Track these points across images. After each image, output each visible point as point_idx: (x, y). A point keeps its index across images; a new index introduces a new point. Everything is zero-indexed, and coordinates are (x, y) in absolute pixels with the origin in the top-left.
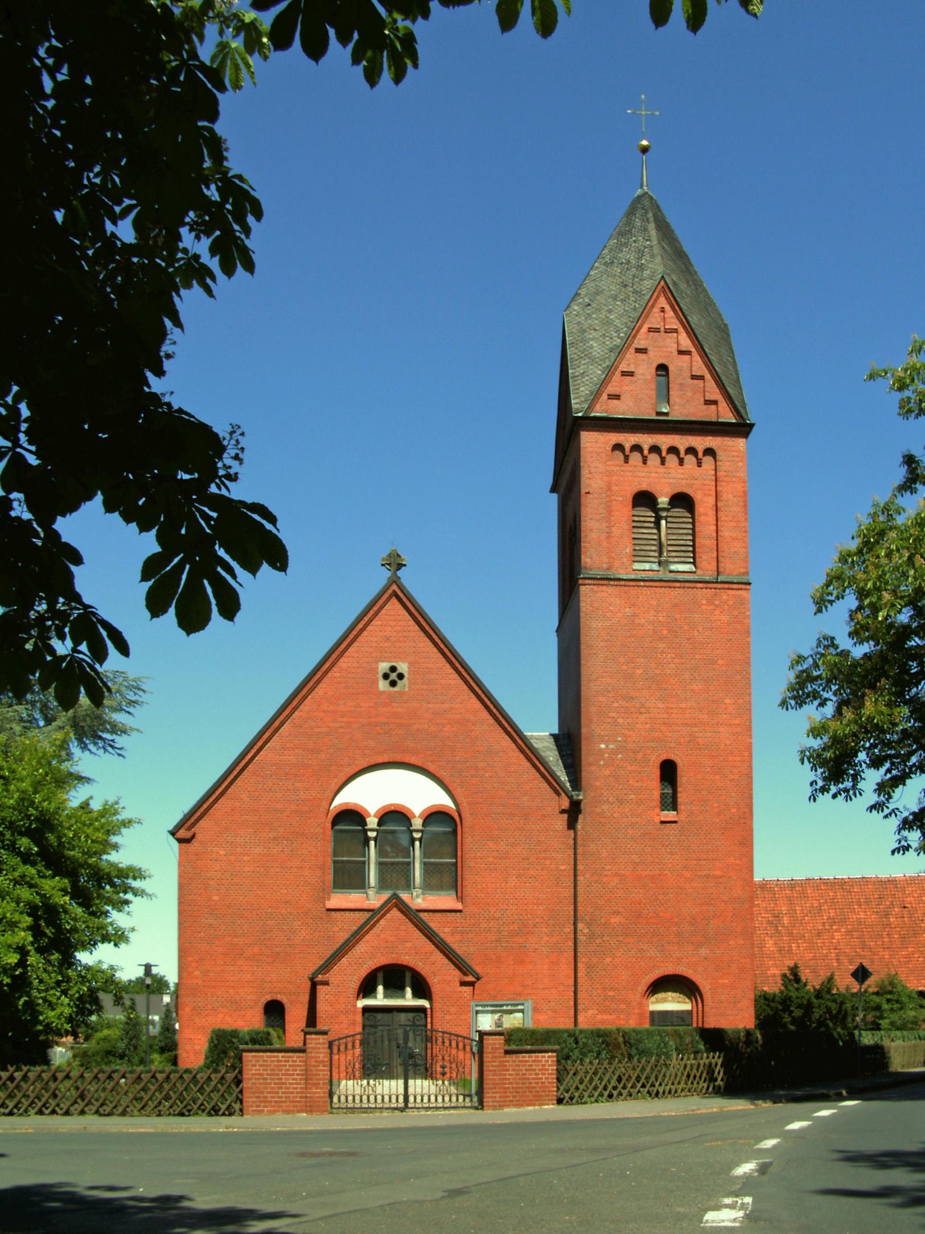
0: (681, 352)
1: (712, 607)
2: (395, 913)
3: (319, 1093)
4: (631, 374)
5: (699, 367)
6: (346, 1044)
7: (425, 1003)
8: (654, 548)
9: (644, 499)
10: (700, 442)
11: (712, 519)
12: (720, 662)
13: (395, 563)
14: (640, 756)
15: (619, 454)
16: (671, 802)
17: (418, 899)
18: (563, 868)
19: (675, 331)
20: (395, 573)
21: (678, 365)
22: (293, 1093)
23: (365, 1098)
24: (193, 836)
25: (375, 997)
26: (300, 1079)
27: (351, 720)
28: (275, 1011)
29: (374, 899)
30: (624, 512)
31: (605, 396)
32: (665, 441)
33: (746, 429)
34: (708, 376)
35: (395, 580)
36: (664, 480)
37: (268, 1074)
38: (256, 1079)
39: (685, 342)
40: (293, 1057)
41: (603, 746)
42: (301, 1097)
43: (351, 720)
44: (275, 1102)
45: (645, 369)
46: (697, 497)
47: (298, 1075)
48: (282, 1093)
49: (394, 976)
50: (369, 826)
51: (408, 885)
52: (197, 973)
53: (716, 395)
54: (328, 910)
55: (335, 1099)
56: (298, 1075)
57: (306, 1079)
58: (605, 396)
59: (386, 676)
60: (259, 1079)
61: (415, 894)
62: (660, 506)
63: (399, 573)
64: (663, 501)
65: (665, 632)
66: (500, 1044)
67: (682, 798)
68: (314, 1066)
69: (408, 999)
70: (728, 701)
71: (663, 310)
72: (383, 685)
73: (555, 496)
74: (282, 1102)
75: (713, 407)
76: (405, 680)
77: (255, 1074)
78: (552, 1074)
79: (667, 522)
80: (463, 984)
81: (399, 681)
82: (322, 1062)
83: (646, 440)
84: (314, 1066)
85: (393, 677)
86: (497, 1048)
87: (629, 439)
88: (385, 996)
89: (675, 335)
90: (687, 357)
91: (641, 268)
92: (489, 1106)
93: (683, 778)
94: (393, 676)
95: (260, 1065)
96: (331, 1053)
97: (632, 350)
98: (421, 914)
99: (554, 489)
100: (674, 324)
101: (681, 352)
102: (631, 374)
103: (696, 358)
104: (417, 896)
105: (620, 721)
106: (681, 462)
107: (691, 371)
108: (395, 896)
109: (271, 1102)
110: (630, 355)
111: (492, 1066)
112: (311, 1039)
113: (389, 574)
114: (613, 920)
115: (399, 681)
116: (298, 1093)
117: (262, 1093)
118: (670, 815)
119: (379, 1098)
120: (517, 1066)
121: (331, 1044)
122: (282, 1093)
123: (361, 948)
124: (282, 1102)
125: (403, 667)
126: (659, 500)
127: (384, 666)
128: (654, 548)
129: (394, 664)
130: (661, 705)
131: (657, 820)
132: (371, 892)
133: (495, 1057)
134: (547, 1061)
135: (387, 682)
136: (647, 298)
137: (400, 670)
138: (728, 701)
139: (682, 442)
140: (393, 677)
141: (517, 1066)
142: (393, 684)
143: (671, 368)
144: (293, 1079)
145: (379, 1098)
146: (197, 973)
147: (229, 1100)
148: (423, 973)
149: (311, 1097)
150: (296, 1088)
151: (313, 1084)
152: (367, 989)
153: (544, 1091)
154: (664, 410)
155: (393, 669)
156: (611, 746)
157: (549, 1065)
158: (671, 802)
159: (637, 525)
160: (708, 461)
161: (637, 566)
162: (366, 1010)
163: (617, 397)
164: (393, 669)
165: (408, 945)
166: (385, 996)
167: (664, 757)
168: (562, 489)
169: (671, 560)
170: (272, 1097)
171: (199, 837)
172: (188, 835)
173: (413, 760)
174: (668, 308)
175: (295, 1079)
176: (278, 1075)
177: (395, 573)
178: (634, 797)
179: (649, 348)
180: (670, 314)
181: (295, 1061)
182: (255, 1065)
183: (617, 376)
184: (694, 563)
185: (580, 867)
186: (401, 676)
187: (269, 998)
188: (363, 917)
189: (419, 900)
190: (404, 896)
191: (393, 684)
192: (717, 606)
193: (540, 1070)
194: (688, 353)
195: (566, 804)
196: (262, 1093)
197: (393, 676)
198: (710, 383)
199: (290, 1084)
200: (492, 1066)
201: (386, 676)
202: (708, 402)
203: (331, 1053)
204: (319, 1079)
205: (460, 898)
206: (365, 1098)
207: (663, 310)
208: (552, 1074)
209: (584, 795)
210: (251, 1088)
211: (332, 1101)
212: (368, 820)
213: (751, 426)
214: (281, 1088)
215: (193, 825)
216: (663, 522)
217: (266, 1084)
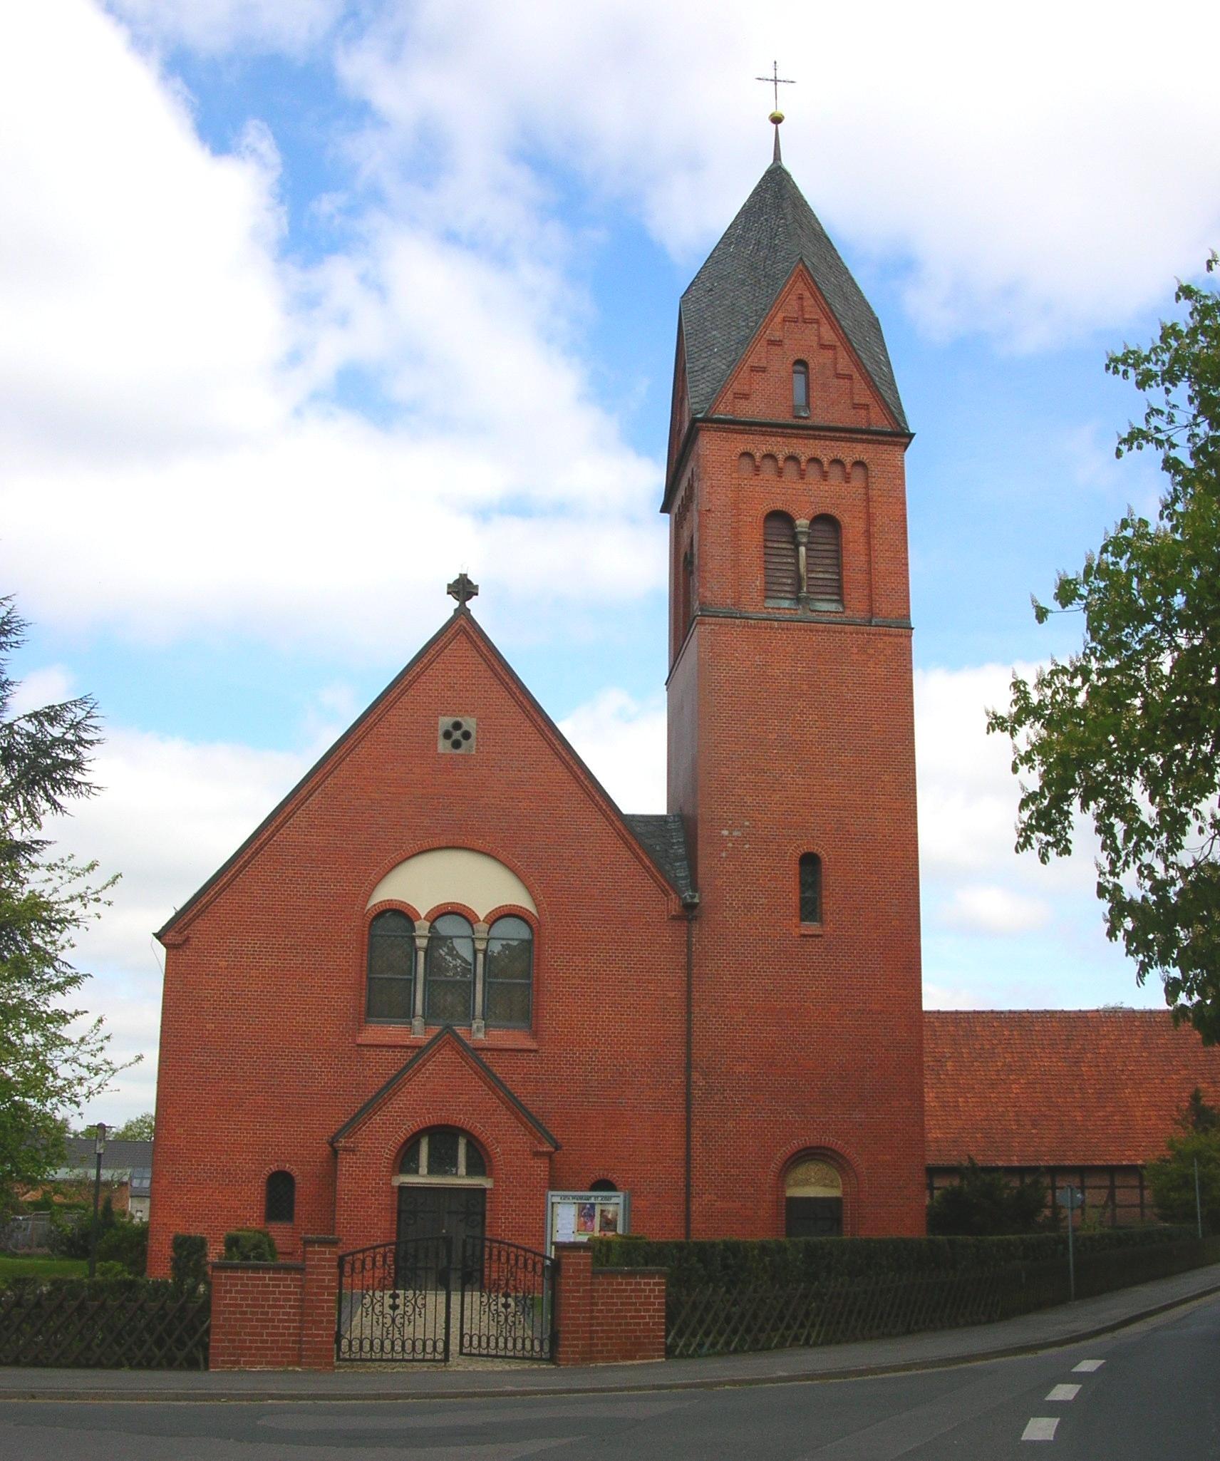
0: (823, 346)
1: (864, 657)
2: (447, 1054)
3: (321, 1336)
4: (763, 370)
5: (844, 364)
6: (363, 1262)
7: (486, 1183)
8: (789, 581)
9: (780, 518)
10: (850, 452)
11: (862, 548)
12: (876, 727)
13: (463, 589)
14: (773, 847)
15: (746, 461)
16: (810, 909)
17: (478, 1034)
18: (672, 995)
19: (817, 322)
20: (463, 604)
21: (817, 361)
22: (284, 1335)
23: (387, 1344)
24: (187, 939)
25: (416, 1172)
26: (295, 1314)
27: (401, 790)
28: (280, 1191)
29: (419, 1032)
30: (753, 537)
31: (730, 395)
32: (805, 449)
33: (906, 440)
34: (856, 375)
35: (462, 613)
36: (805, 498)
37: (248, 1306)
38: (230, 1312)
39: (828, 335)
40: (286, 1279)
41: (725, 833)
42: (294, 1342)
43: (401, 790)
44: (258, 1349)
45: (780, 364)
46: (845, 519)
47: (291, 1307)
48: (268, 1334)
49: (443, 1138)
50: (418, 933)
51: (468, 1015)
52: (179, 1130)
53: (863, 396)
54: (359, 1045)
55: (345, 1342)
56: (291, 1307)
57: (302, 1314)
58: (730, 395)
59: (447, 735)
60: (234, 1313)
61: (475, 1026)
62: (799, 529)
63: (468, 604)
64: (802, 523)
65: (805, 687)
66: (585, 1264)
67: (829, 905)
68: (316, 1294)
69: (460, 1178)
70: (886, 778)
71: (801, 298)
72: (443, 746)
73: (667, 516)
74: (267, 1348)
75: (863, 412)
76: (472, 740)
77: (231, 1305)
78: (659, 1310)
79: (807, 550)
80: (537, 1154)
81: (464, 742)
82: (327, 1288)
83: (781, 447)
84: (316, 1294)
85: (457, 735)
86: (581, 1271)
87: (760, 446)
88: (431, 1172)
89: (815, 326)
90: (830, 353)
91: (774, 249)
92: (568, 1360)
93: (832, 878)
94: (457, 735)
95: (237, 1292)
96: (341, 1274)
97: (763, 342)
98: (483, 1055)
99: (665, 509)
100: (812, 311)
101: (823, 346)
102: (763, 370)
103: (842, 353)
104: (478, 1029)
105: (748, 799)
106: (825, 476)
107: (836, 369)
108: (448, 1028)
109: (250, 1348)
110: (761, 348)
111: (574, 1298)
112: (314, 1253)
113: (456, 604)
114: (738, 1069)
115: (464, 742)
116: (290, 1335)
117: (238, 1334)
118: (812, 927)
119: (409, 1344)
120: (609, 1297)
121: (341, 1260)
122: (268, 1334)
123: (400, 1102)
124: (267, 1348)
125: (470, 723)
126: (798, 522)
127: (445, 722)
128: (789, 581)
129: (459, 719)
130: (800, 780)
131: (796, 932)
132: (418, 1023)
133: (578, 1284)
134: (651, 1290)
135: (448, 743)
136: (781, 283)
137: (465, 728)
138: (886, 778)
139: (825, 451)
140: (457, 735)
141: (609, 1297)
142: (457, 745)
143: (811, 365)
144: (284, 1314)
145: (409, 1344)
146: (179, 1130)
147: (190, 1344)
148: (483, 1138)
149: (308, 1342)
150: (288, 1328)
151: (314, 1322)
152: (405, 1159)
153: (648, 1337)
154: (803, 414)
155: (457, 726)
156: (735, 833)
157: (655, 1297)
158: (810, 909)
159: (768, 552)
160: (858, 474)
161: (770, 603)
162: (402, 1189)
163: (746, 396)
164: (457, 726)
165: (464, 1098)
166: (431, 1172)
167: (805, 849)
168: (675, 509)
169: (812, 596)
170: (251, 1341)
171: (194, 942)
172: (180, 939)
173: (479, 844)
174: (807, 294)
175: (288, 1314)
176: (263, 1306)
177: (463, 604)
178: (763, 901)
179: (786, 341)
180: (809, 302)
181: (289, 1286)
182: (230, 1292)
183: (745, 373)
184: (840, 601)
185: (696, 995)
186: (467, 735)
187: (274, 1168)
188: (403, 1057)
189: (481, 1036)
190: (460, 1030)
191: (457, 745)
192: (871, 656)
193: (641, 1304)
194: (833, 348)
195: (675, 907)
196: (238, 1334)
197: (457, 735)
198: (860, 385)
199: (280, 1321)
200: (574, 1298)
201: (447, 735)
202: (856, 406)
203: (341, 1274)
204: (322, 1315)
205: (535, 1034)
206: (387, 1344)
207: (801, 298)
208: (659, 1310)
209: (700, 898)
210: (222, 1326)
211: (339, 1349)
212: (417, 924)
213: (911, 436)
214: (267, 1327)
215: (188, 925)
216: (802, 549)
217: (244, 1320)
